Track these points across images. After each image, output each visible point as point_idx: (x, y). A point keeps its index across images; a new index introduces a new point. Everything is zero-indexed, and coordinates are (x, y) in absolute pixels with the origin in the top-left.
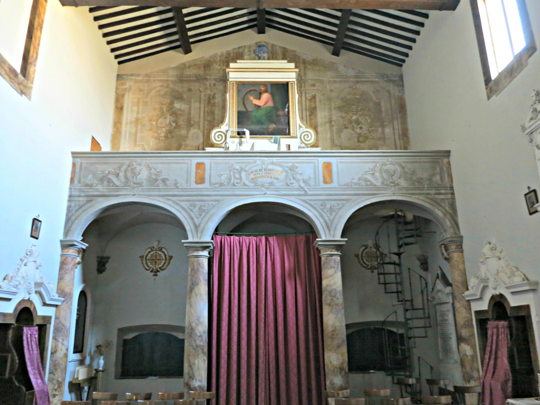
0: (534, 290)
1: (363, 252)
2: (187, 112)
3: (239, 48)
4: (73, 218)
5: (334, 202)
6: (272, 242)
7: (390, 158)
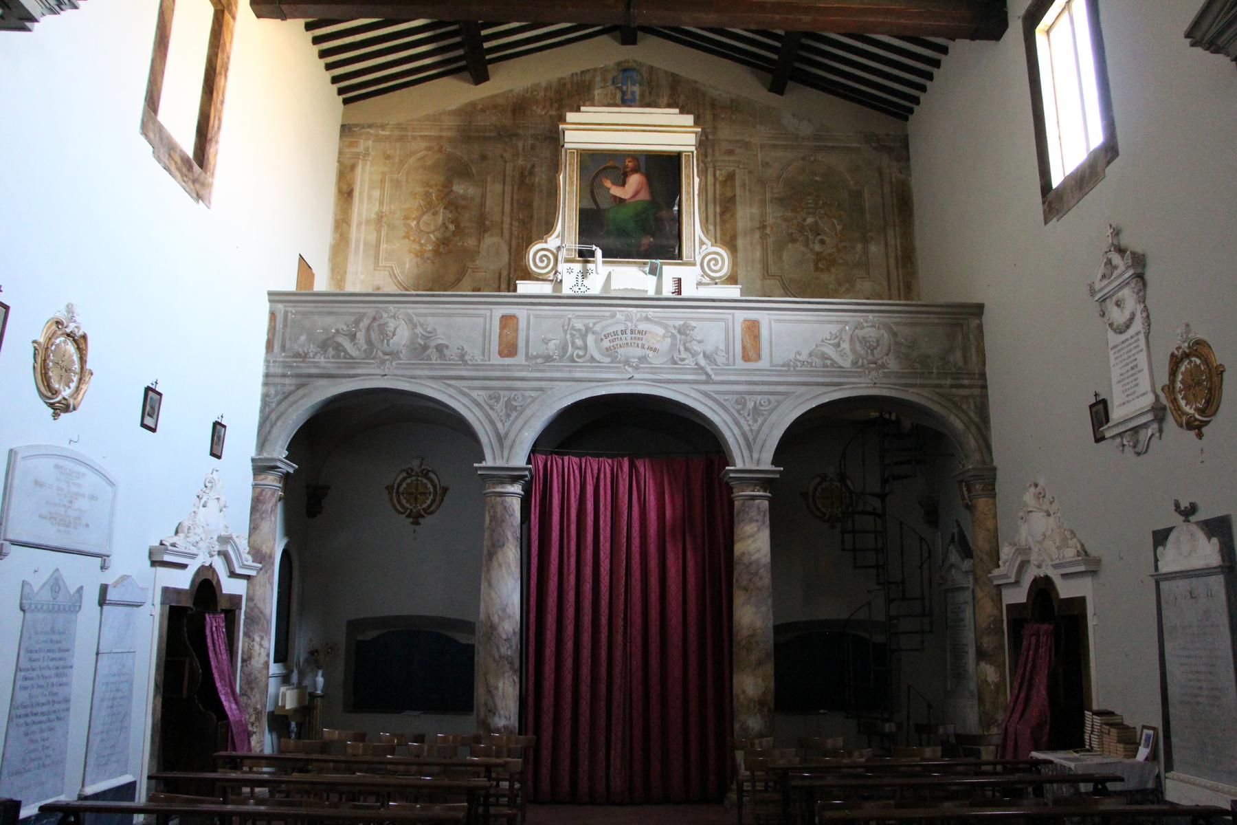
0: (1094, 573)
1: (816, 488)
2: (478, 200)
3: (583, 72)
4: (273, 417)
5: (760, 397)
6: (642, 470)
7: (870, 316)
